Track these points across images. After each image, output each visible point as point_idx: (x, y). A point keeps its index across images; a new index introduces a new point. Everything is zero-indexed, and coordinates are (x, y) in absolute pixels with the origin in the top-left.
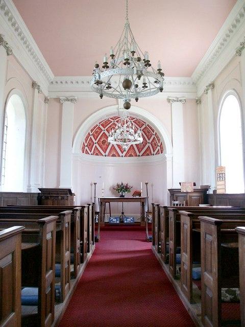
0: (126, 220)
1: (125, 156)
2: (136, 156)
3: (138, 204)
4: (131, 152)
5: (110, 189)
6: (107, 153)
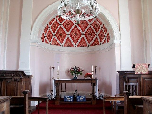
0: (79, 99)
1: (78, 46)
2: (86, 46)
3: (90, 85)
5: (66, 72)
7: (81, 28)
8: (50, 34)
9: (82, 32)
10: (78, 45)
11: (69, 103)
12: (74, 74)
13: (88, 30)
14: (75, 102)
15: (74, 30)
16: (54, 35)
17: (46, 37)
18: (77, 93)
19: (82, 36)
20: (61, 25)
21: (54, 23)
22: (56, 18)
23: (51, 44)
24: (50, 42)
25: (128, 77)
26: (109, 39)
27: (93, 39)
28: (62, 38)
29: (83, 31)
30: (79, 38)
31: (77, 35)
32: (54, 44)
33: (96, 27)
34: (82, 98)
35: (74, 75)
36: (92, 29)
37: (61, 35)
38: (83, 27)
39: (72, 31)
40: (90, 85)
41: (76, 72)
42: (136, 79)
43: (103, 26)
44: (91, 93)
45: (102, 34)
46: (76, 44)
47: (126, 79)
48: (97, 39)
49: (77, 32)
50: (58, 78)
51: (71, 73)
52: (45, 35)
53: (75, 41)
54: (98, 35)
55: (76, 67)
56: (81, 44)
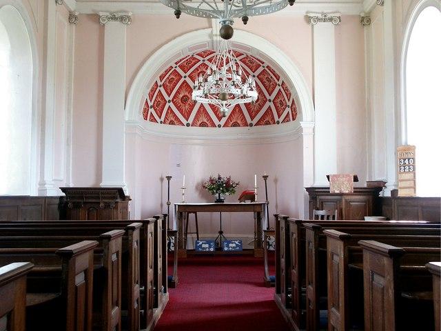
0: (228, 246)
1: (226, 125)
2: (246, 124)
3: (249, 216)
5: (197, 188)
8: (160, 100)
10: (226, 123)
11: (208, 254)
14: (218, 252)
16: (169, 101)
18: (222, 238)
20: (185, 77)
22: (174, 66)
23: (161, 122)
25: (346, 201)
27: (260, 108)
32: (169, 122)
33: (267, 83)
34: (234, 245)
35: (217, 195)
40: (249, 216)
44: (252, 236)
45: (281, 101)
47: (318, 203)
48: (271, 110)
50: (183, 202)
51: (209, 189)
52: (150, 104)
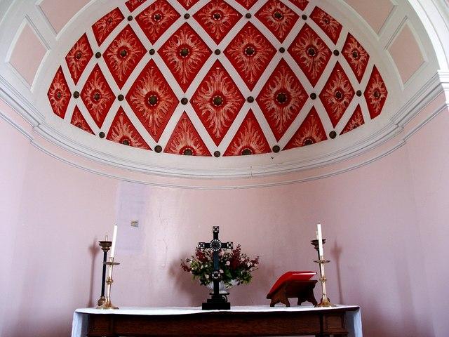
1: (229, 152)
2: (266, 149)
4: (250, 140)
5: (172, 271)
6: (163, 142)
7: (239, 71)
9: (246, 92)
12: (211, 278)
13: (271, 82)
15: (209, 80)
17: (76, 95)
19: (246, 108)
21: (118, 38)
24: (100, 124)
26: (383, 100)
27: (293, 117)
28: (156, 116)
29: (251, 87)
30: (232, 116)
31: (225, 103)
32: (119, 138)
33: (308, 61)
35: (211, 285)
36: (291, 73)
37: (152, 100)
38: (250, 67)
39: (203, 85)
41: (222, 271)
42: (324, 318)
43: (346, 46)
46: (217, 142)
49: (225, 92)
53: (214, 131)
54: (340, 51)
55: (222, 239)
56: (244, 144)
